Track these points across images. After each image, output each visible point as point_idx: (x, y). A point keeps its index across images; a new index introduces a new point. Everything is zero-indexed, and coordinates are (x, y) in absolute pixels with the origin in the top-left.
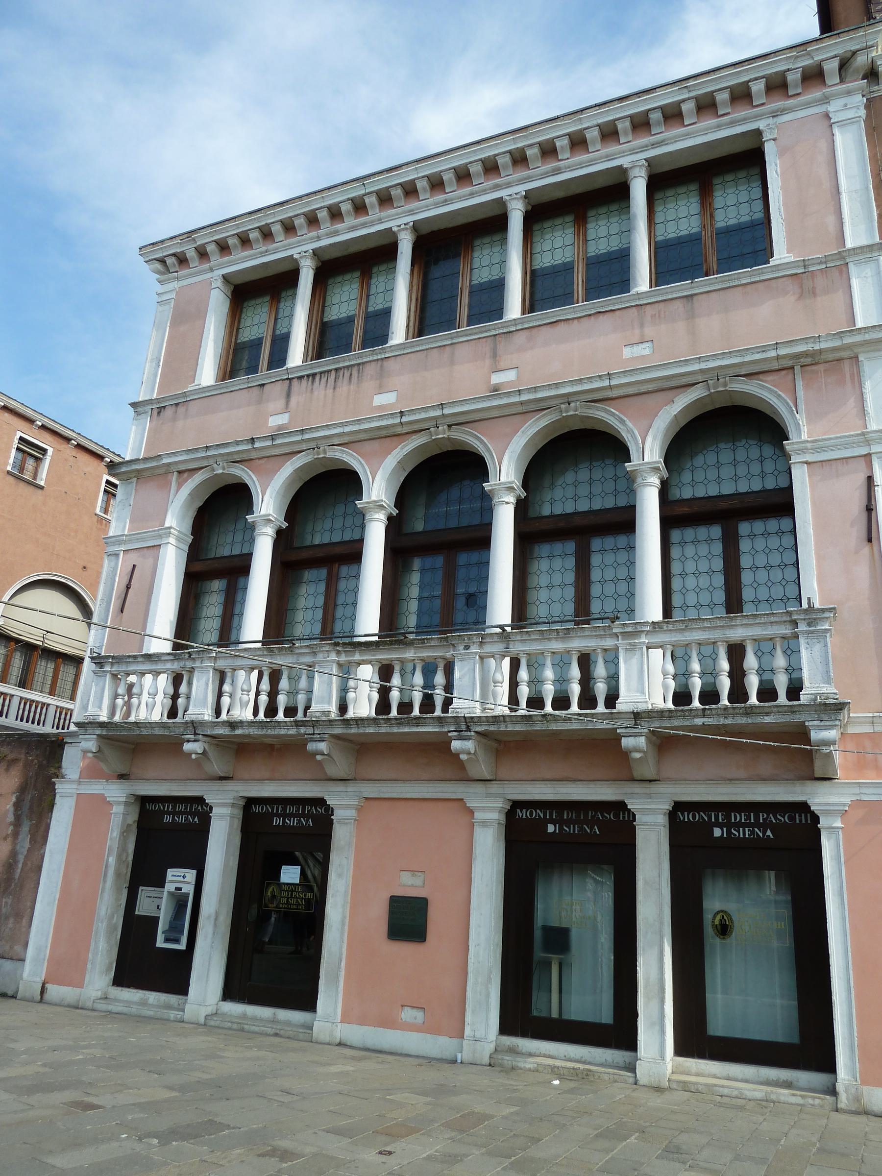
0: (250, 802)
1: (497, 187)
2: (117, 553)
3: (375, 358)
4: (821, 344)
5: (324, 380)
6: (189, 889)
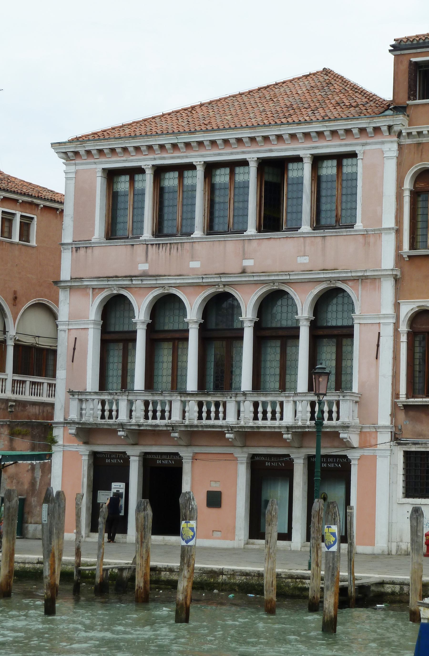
0: (146, 454)
1: (243, 153)
2: (65, 330)
3: (189, 241)
4: (367, 273)
5: (164, 248)
6: (123, 491)
